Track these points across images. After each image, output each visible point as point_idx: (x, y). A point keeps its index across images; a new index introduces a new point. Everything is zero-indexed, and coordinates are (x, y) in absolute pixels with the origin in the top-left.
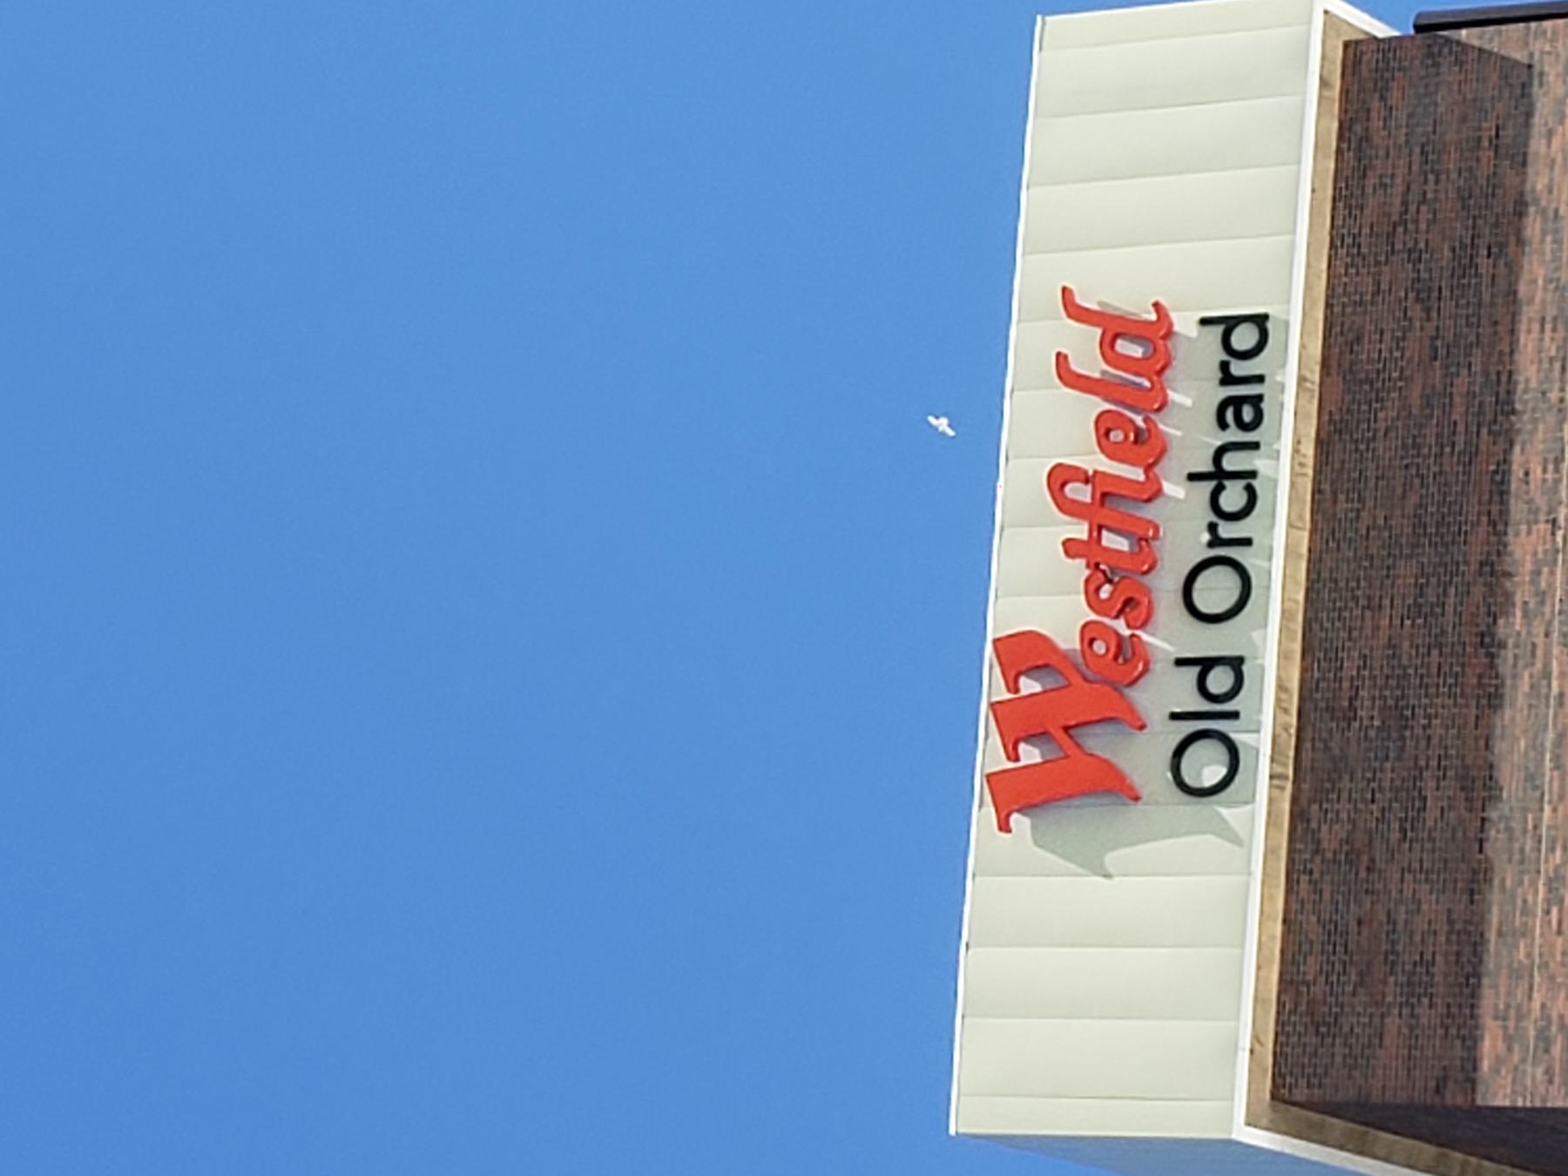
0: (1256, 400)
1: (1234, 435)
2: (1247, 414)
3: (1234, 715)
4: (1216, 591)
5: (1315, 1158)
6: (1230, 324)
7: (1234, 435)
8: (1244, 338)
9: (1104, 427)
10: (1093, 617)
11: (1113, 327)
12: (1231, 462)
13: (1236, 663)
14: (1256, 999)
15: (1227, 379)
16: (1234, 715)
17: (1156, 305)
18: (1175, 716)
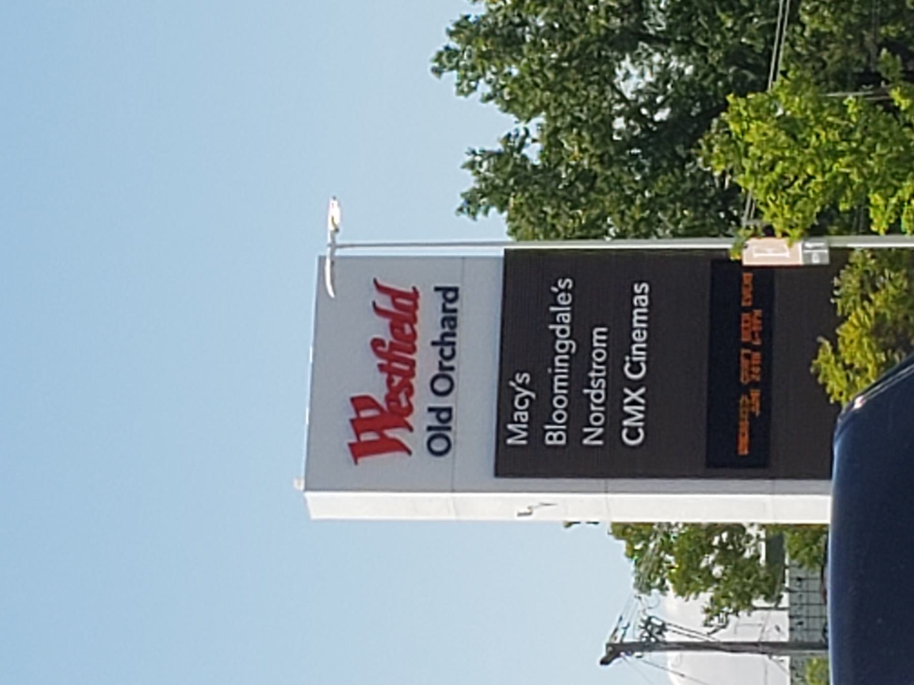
1: (447, 330)
6: (444, 290)
9: (392, 327)
11: (394, 294)
12: (448, 339)
15: (445, 310)
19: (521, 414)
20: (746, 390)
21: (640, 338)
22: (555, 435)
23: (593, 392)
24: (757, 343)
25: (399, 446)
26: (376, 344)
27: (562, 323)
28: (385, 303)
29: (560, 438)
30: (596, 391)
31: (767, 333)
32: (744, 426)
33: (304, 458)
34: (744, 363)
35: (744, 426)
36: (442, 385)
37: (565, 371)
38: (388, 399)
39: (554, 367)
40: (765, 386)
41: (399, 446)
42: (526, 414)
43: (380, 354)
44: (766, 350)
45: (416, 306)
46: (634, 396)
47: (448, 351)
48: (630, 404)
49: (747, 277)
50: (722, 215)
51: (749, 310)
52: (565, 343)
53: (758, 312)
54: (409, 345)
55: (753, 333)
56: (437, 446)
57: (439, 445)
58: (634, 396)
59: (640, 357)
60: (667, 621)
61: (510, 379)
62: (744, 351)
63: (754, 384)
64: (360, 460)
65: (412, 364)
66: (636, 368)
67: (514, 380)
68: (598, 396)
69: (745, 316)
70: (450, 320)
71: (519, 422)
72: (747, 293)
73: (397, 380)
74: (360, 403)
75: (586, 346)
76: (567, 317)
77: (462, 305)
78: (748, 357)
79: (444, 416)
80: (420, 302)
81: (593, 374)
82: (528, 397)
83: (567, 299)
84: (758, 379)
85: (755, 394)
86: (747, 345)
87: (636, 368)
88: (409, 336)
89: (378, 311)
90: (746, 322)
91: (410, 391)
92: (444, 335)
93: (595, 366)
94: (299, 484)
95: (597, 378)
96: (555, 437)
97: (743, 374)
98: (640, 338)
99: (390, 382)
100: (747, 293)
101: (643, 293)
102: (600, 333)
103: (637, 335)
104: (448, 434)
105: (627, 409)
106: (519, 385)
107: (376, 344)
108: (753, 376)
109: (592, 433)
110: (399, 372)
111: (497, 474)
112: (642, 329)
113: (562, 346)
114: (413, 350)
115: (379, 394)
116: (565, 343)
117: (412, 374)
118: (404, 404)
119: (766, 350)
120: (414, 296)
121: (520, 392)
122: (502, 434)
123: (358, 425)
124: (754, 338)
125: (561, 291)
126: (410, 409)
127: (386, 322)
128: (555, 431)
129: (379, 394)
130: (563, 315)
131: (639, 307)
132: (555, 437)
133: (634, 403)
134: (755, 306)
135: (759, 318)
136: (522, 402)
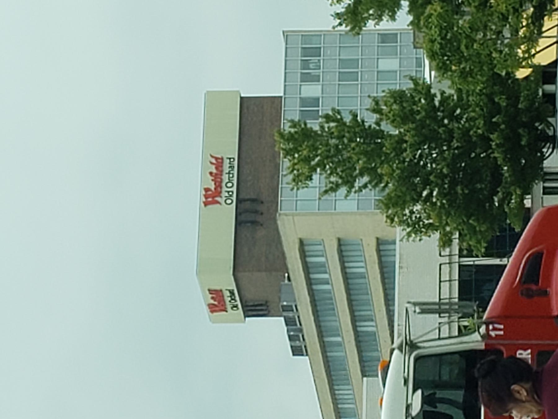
11: (216, 159)
25: (218, 202)
28: (214, 161)
33: (223, 325)
38: (215, 189)
41: (218, 202)
49: (554, 70)
50: (458, 111)
56: (228, 202)
60: (345, 201)
73: (217, 184)
74: (207, 190)
79: (231, 193)
89: (212, 163)
91: (221, 188)
104: (233, 181)
115: (213, 187)
123: (206, 197)
127: (214, 167)
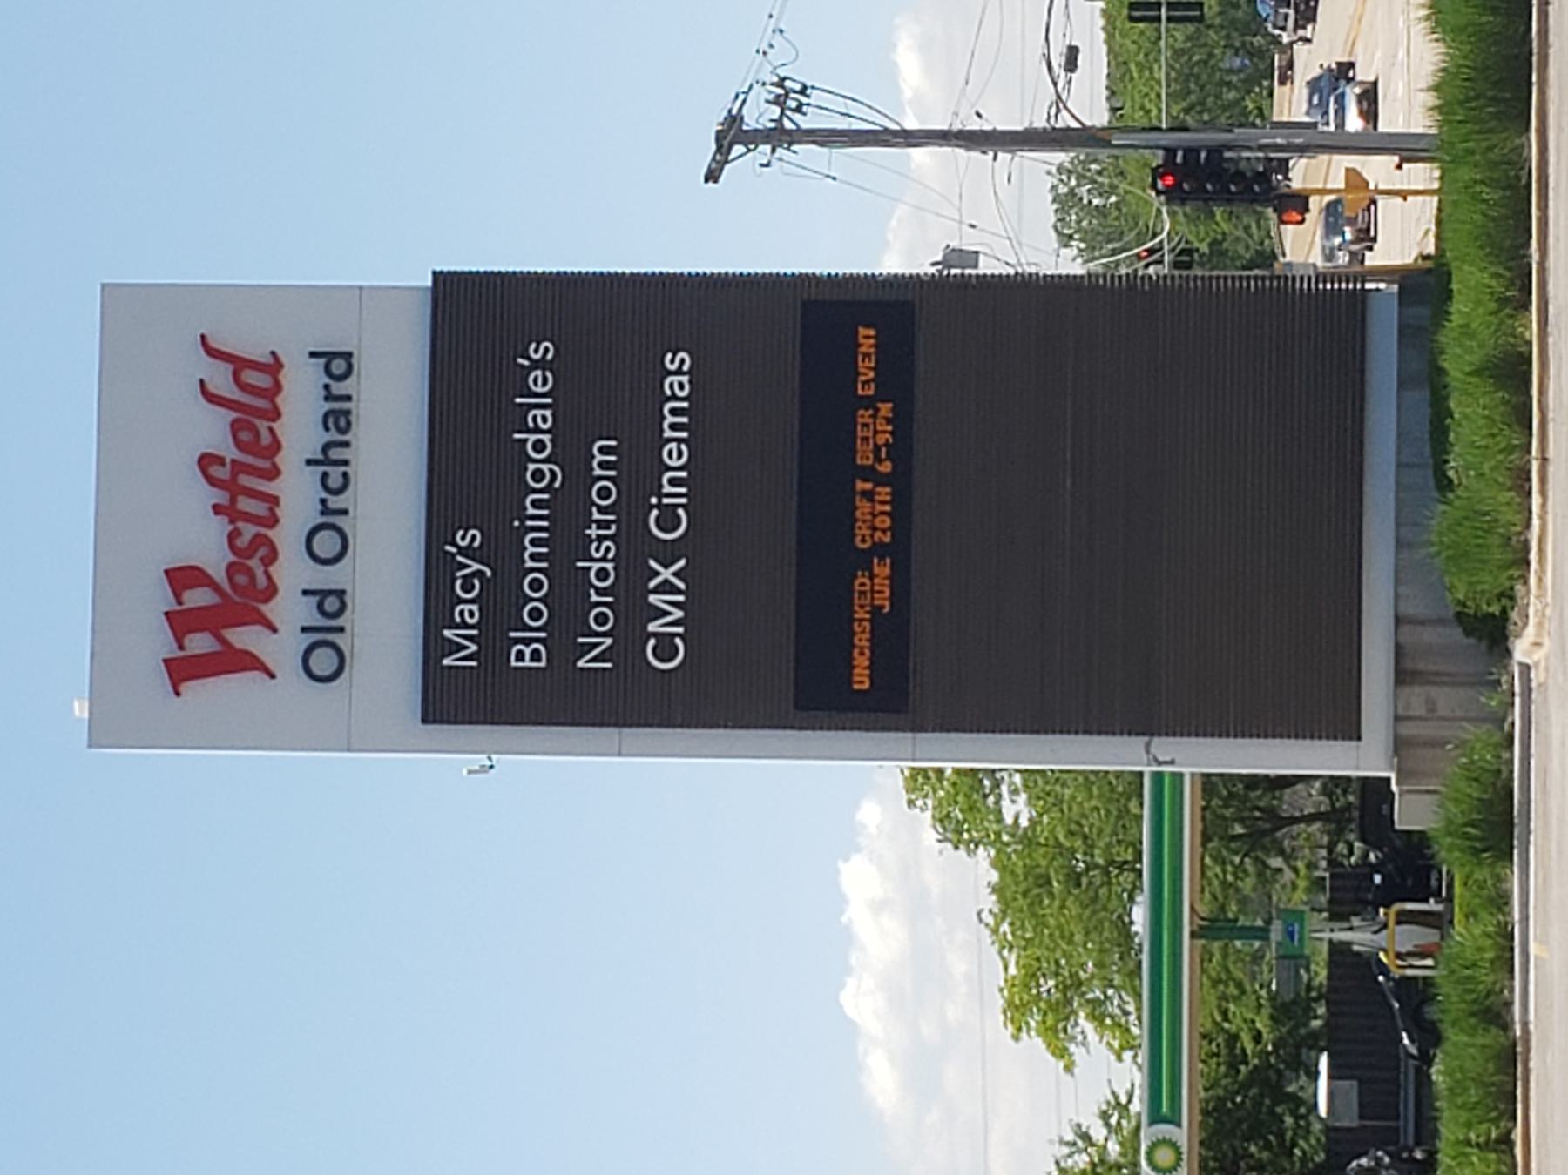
0: (347, 413)
1: (334, 436)
2: (342, 423)
3: (341, 630)
4: (326, 544)
5: (260, 481)
6: (330, 356)
7: (334, 436)
8: (338, 366)
9: (235, 427)
10: (270, 533)
11: (239, 364)
12: (335, 454)
13: (340, 594)
14: (349, 750)
15: (329, 397)
16: (341, 630)
17: (273, 353)
18: (304, 630)
19: (466, 607)
20: (864, 561)
21: (675, 456)
22: (527, 651)
23: (596, 566)
24: (886, 467)
25: (248, 662)
26: (206, 462)
27: (537, 430)
29: (536, 656)
30: (600, 561)
31: (901, 449)
32: (862, 639)
34: (863, 507)
35: (862, 639)
36: (326, 544)
37: (545, 524)
39: (524, 518)
40: (899, 551)
41: (248, 662)
42: (475, 608)
43: (212, 481)
44: (901, 482)
45: (278, 387)
46: (667, 574)
47: (335, 474)
48: (656, 591)
51: (869, 403)
52: (542, 470)
53: (885, 408)
54: (265, 464)
55: (877, 448)
57: (323, 661)
58: (667, 574)
59: (674, 494)
61: (446, 543)
62: (861, 485)
63: (879, 550)
64: (183, 687)
65: (274, 501)
66: (668, 520)
67: (454, 544)
68: (604, 574)
69: (864, 416)
70: (338, 418)
71: (465, 626)
72: (866, 370)
74: (182, 578)
75: (579, 475)
76: (543, 417)
77: (355, 435)
78: (869, 496)
80: (286, 377)
81: (593, 532)
82: (480, 574)
83: (545, 382)
84: (887, 539)
85: (882, 570)
86: (869, 473)
87: (668, 520)
88: (267, 448)
90: (866, 425)
91: (272, 556)
92: (326, 447)
93: (596, 516)
94: (81, 710)
95: (601, 539)
96: (527, 656)
97: (862, 530)
98: (675, 456)
99: (232, 537)
100: (866, 370)
101: (679, 372)
102: (602, 450)
103: (670, 453)
105: (653, 599)
106: (461, 551)
107: (206, 462)
108: (878, 534)
109: (597, 645)
110: (249, 518)
111: (425, 721)
112: (679, 441)
113: (540, 475)
114: (273, 473)
115: (213, 555)
116: (542, 470)
117: (273, 521)
118: (262, 581)
119: (901, 482)
120: (274, 366)
121: (467, 566)
122: (434, 646)
123: (180, 623)
124: (878, 460)
125: (536, 365)
126: (271, 591)
128: (527, 642)
129: (213, 555)
130: (539, 412)
131: (675, 398)
132: (527, 656)
133: (667, 588)
134: (880, 397)
135: (888, 421)
136: (467, 588)
